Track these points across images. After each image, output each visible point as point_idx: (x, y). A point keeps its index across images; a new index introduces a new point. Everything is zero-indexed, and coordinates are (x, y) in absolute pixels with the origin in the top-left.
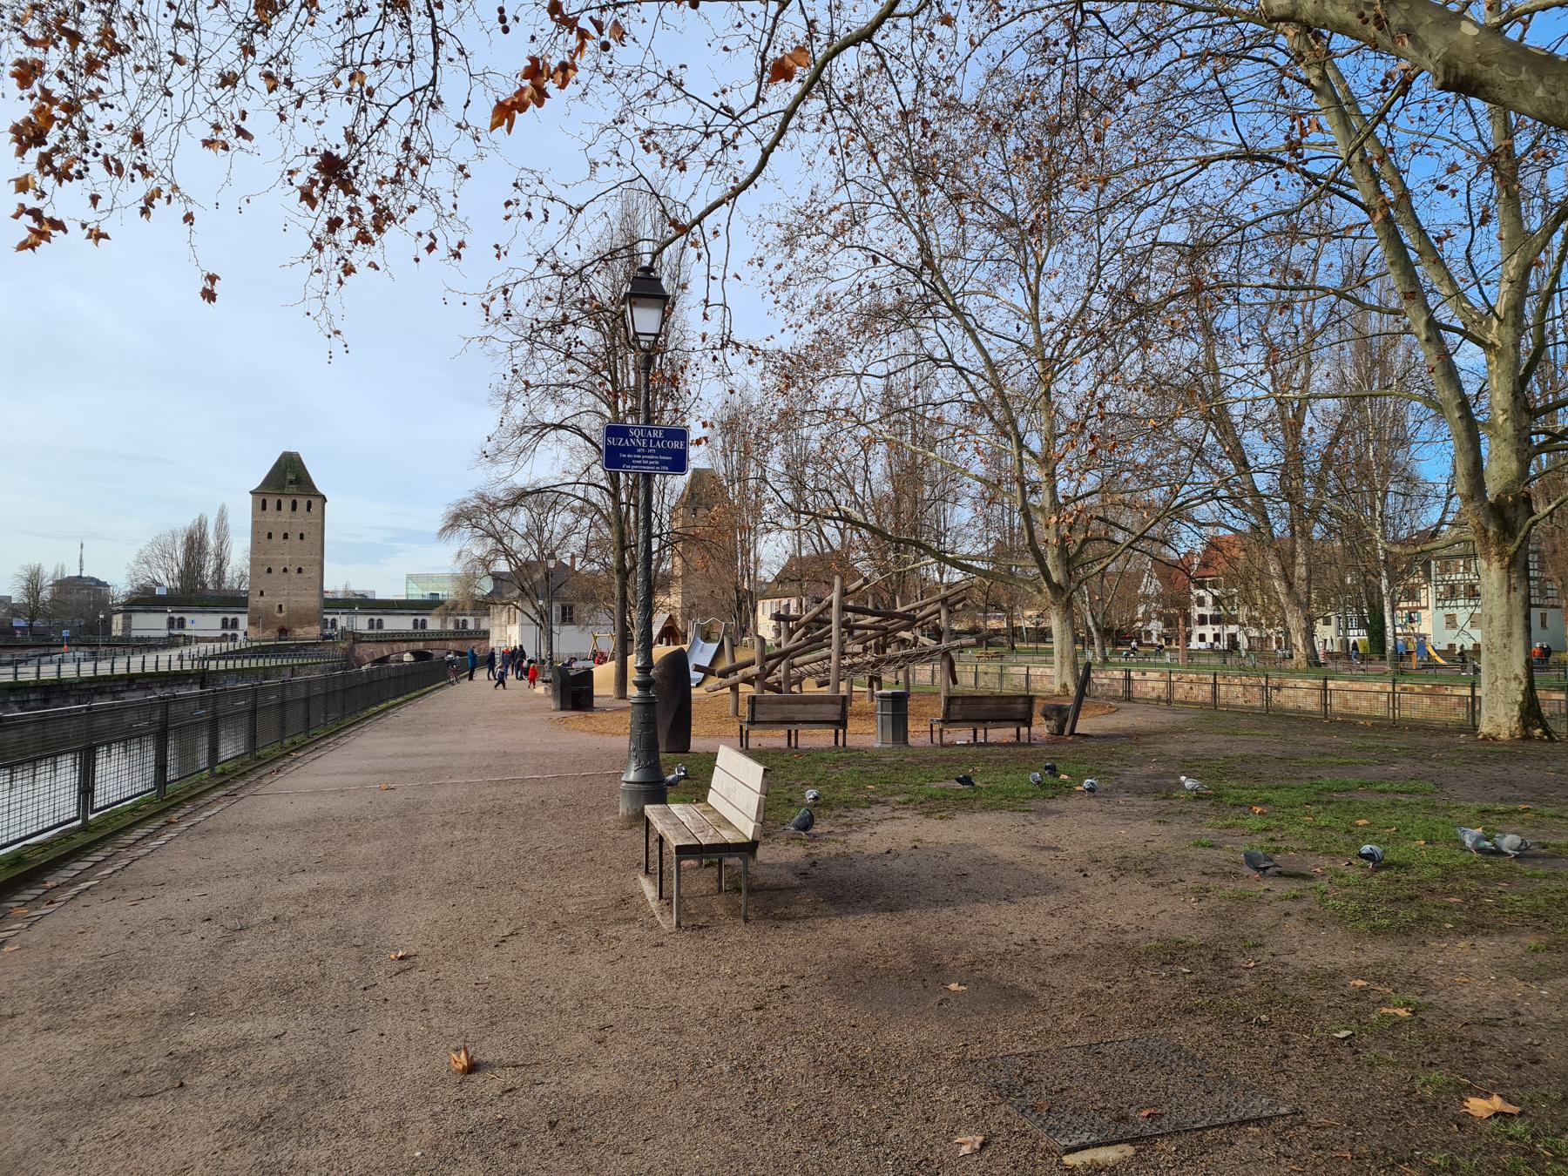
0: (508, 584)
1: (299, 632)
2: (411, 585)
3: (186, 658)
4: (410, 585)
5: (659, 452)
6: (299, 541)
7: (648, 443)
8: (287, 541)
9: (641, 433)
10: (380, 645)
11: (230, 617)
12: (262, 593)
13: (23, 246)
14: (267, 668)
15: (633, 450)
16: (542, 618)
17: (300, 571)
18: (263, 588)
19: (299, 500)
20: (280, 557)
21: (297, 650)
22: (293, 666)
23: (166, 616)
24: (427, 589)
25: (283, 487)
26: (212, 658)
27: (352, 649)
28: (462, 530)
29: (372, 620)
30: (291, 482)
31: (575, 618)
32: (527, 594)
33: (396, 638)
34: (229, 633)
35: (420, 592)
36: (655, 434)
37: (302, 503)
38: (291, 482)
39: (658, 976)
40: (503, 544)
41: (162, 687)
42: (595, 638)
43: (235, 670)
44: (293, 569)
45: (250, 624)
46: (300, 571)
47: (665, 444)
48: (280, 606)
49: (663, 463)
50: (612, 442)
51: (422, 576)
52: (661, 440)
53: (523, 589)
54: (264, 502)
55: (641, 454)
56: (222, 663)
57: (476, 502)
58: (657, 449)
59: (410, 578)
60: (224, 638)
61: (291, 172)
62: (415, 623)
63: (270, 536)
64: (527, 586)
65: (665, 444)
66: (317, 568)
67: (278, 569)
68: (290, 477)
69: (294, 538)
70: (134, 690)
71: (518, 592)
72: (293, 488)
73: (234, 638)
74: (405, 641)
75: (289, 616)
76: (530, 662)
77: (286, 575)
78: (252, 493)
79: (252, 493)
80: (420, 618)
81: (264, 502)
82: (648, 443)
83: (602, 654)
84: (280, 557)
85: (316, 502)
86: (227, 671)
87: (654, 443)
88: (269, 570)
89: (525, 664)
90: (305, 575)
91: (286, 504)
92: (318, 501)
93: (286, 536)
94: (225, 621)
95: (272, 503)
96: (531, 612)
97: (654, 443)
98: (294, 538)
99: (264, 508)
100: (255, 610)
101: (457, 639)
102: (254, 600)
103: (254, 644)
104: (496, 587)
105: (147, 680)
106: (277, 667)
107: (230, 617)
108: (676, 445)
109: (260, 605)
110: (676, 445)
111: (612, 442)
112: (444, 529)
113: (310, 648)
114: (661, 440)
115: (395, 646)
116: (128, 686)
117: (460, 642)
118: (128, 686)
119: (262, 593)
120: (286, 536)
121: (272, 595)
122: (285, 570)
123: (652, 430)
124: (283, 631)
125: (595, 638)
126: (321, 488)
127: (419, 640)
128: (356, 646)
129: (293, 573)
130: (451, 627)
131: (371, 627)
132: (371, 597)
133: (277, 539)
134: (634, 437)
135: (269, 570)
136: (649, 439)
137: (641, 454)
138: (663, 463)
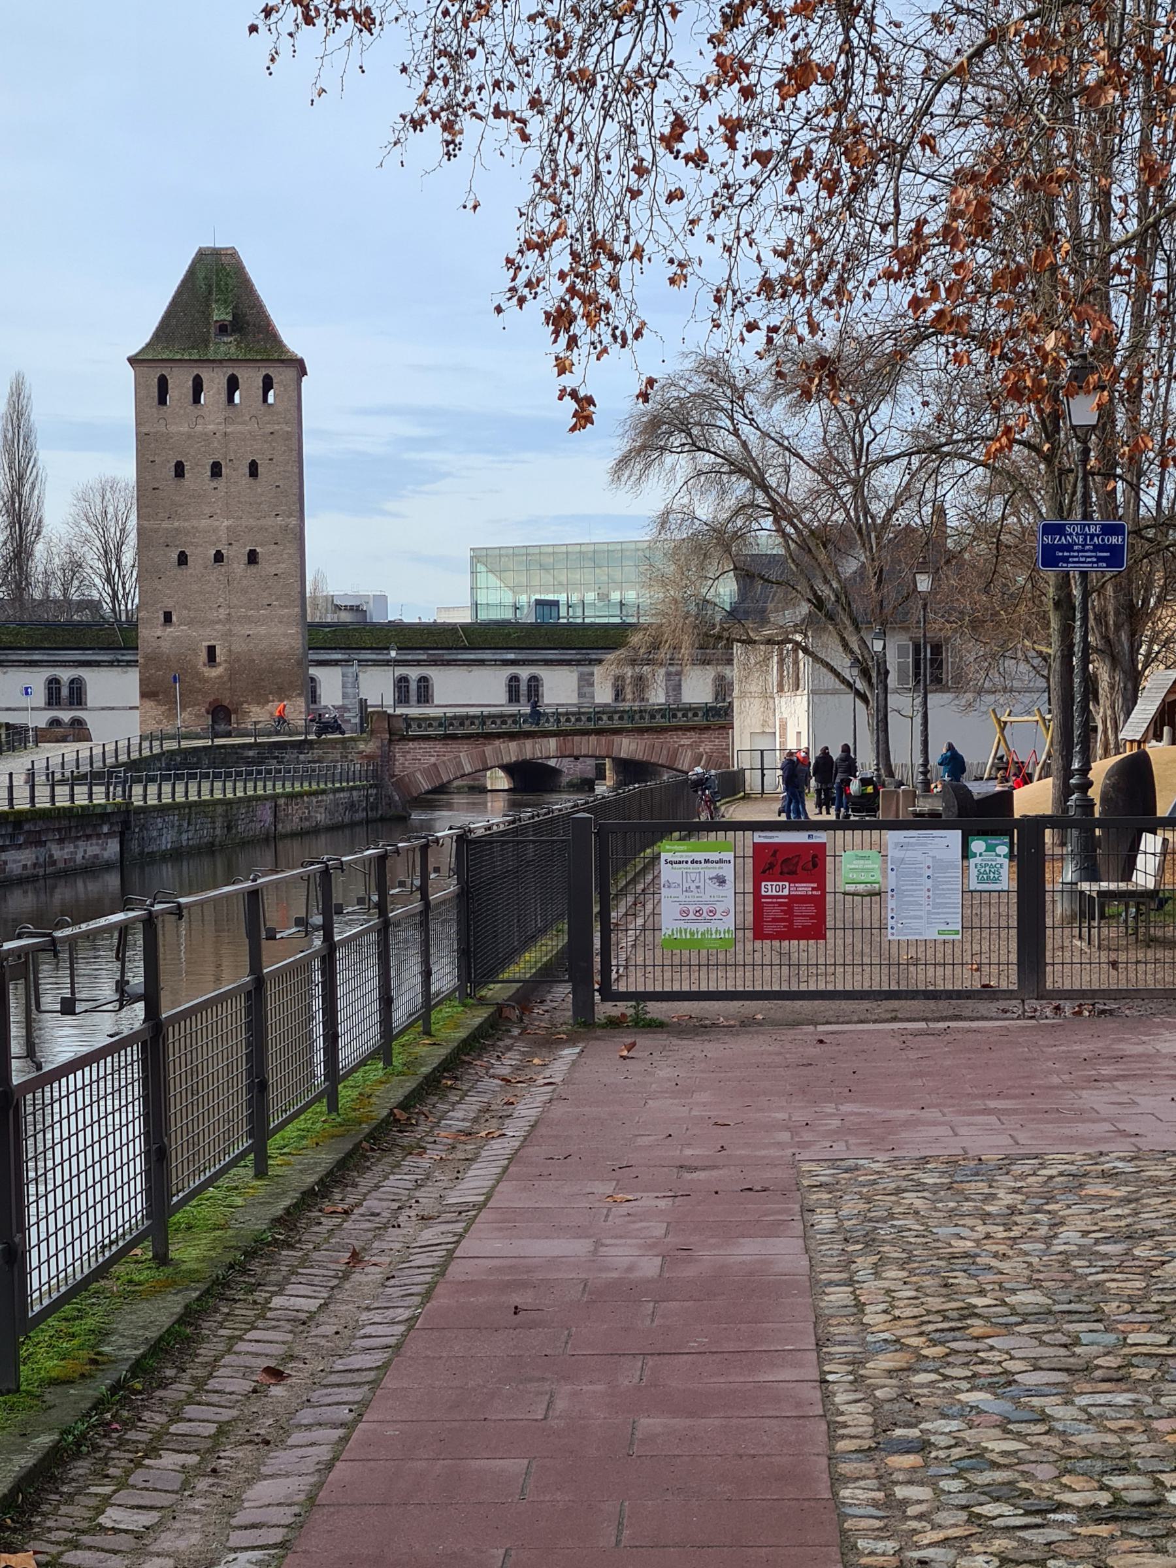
0: (780, 592)
1: (259, 714)
2: (488, 580)
3: (40, 779)
4: (482, 580)
5: (1097, 548)
6: (246, 480)
7: (1085, 539)
8: (221, 483)
9: (1078, 529)
10: (453, 746)
11: (65, 675)
12: (168, 618)
13: (573, 429)
14: (227, 803)
15: (1069, 547)
16: (865, 673)
17: (252, 558)
18: (169, 604)
19: (243, 374)
20: (204, 523)
21: (260, 760)
22: (275, 797)
23: (37, 679)
24: (528, 588)
25: (206, 342)
26: (76, 780)
27: (387, 758)
28: (669, 459)
29: (514, 679)
30: (223, 329)
31: (947, 676)
32: (830, 617)
33: (492, 728)
34: (66, 716)
35: (508, 598)
36: (1092, 530)
37: (250, 378)
38: (223, 329)
39: (959, 34)
40: (766, 488)
41: (61, 841)
42: (1003, 726)
43: (174, 807)
44: (236, 555)
45: (143, 695)
46: (252, 558)
47: (1103, 540)
48: (211, 650)
49: (1100, 559)
50: (1048, 540)
51: (514, 552)
52: (1098, 536)
53: (819, 603)
54: (163, 384)
55: (1078, 551)
56: (81, 791)
57: (699, 383)
58: (1094, 545)
59: (479, 557)
60: (55, 732)
61: (692, 222)
62: (513, 685)
63: (180, 471)
64: (825, 591)
65: (1103, 540)
66: (292, 550)
67: (200, 556)
68: (220, 314)
69: (236, 474)
70: (19, 847)
71: (805, 608)
72: (227, 346)
73: (78, 731)
74: (512, 736)
75: (232, 674)
76: (865, 782)
77: (222, 569)
78: (132, 361)
79: (132, 361)
80: (524, 673)
81: (163, 384)
82: (1085, 539)
83: (1020, 766)
84: (204, 523)
85: (281, 375)
86: (162, 809)
87: (1092, 539)
88: (183, 559)
89: (854, 787)
90: (266, 567)
91: (214, 382)
92: (287, 374)
93: (216, 470)
94: (53, 685)
95: (180, 384)
96: (842, 662)
97: (1092, 539)
98: (236, 474)
99: (162, 401)
100: (154, 659)
101: (641, 731)
102: (151, 635)
103: (171, 745)
104: (743, 592)
105: (41, 825)
106: (250, 799)
107: (65, 675)
108: (1114, 540)
109: (165, 646)
110: (1114, 540)
111: (1048, 540)
112: (624, 461)
113: (290, 755)
114: (1098, 536)
115: (489, 750)
116: (12, 837)
117: (648, 739)
118: (12, 837)
119: (168, 618)
120: (216, 470)
121: (190, 623)
122: (219, 557)
123: (1089, 525)
124: (221, 713)
125: (1003, 726)
126: (293, 339)
127: (547, 734)
128: (397, 749)
129: (238, 566)
130: (603, 695)
131: (402, 697)
132: (377, 618)
133: (195, 477)
134: (1071, 534)
135: (183, 559)
136: (1086, 535)
137: (1078, 551)
138: (1100, 559)
